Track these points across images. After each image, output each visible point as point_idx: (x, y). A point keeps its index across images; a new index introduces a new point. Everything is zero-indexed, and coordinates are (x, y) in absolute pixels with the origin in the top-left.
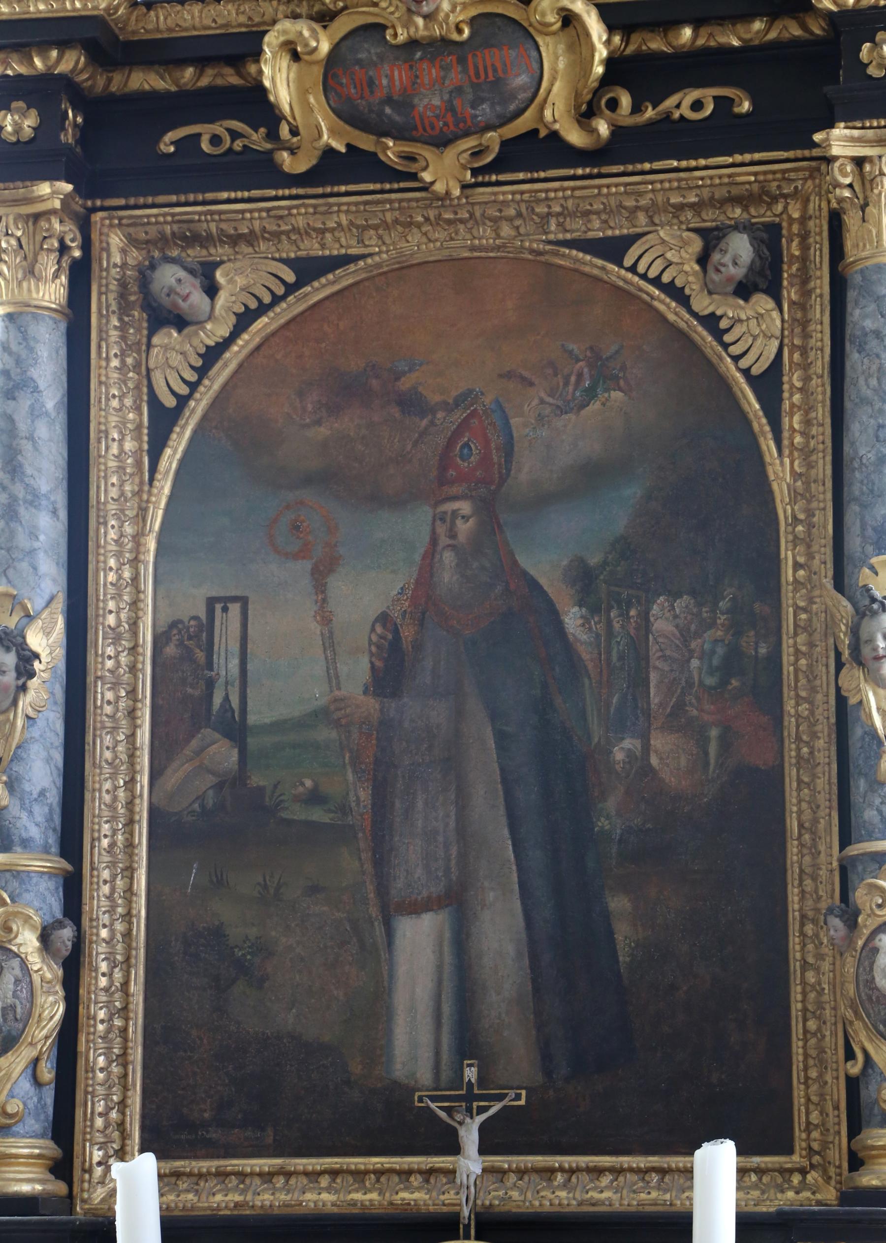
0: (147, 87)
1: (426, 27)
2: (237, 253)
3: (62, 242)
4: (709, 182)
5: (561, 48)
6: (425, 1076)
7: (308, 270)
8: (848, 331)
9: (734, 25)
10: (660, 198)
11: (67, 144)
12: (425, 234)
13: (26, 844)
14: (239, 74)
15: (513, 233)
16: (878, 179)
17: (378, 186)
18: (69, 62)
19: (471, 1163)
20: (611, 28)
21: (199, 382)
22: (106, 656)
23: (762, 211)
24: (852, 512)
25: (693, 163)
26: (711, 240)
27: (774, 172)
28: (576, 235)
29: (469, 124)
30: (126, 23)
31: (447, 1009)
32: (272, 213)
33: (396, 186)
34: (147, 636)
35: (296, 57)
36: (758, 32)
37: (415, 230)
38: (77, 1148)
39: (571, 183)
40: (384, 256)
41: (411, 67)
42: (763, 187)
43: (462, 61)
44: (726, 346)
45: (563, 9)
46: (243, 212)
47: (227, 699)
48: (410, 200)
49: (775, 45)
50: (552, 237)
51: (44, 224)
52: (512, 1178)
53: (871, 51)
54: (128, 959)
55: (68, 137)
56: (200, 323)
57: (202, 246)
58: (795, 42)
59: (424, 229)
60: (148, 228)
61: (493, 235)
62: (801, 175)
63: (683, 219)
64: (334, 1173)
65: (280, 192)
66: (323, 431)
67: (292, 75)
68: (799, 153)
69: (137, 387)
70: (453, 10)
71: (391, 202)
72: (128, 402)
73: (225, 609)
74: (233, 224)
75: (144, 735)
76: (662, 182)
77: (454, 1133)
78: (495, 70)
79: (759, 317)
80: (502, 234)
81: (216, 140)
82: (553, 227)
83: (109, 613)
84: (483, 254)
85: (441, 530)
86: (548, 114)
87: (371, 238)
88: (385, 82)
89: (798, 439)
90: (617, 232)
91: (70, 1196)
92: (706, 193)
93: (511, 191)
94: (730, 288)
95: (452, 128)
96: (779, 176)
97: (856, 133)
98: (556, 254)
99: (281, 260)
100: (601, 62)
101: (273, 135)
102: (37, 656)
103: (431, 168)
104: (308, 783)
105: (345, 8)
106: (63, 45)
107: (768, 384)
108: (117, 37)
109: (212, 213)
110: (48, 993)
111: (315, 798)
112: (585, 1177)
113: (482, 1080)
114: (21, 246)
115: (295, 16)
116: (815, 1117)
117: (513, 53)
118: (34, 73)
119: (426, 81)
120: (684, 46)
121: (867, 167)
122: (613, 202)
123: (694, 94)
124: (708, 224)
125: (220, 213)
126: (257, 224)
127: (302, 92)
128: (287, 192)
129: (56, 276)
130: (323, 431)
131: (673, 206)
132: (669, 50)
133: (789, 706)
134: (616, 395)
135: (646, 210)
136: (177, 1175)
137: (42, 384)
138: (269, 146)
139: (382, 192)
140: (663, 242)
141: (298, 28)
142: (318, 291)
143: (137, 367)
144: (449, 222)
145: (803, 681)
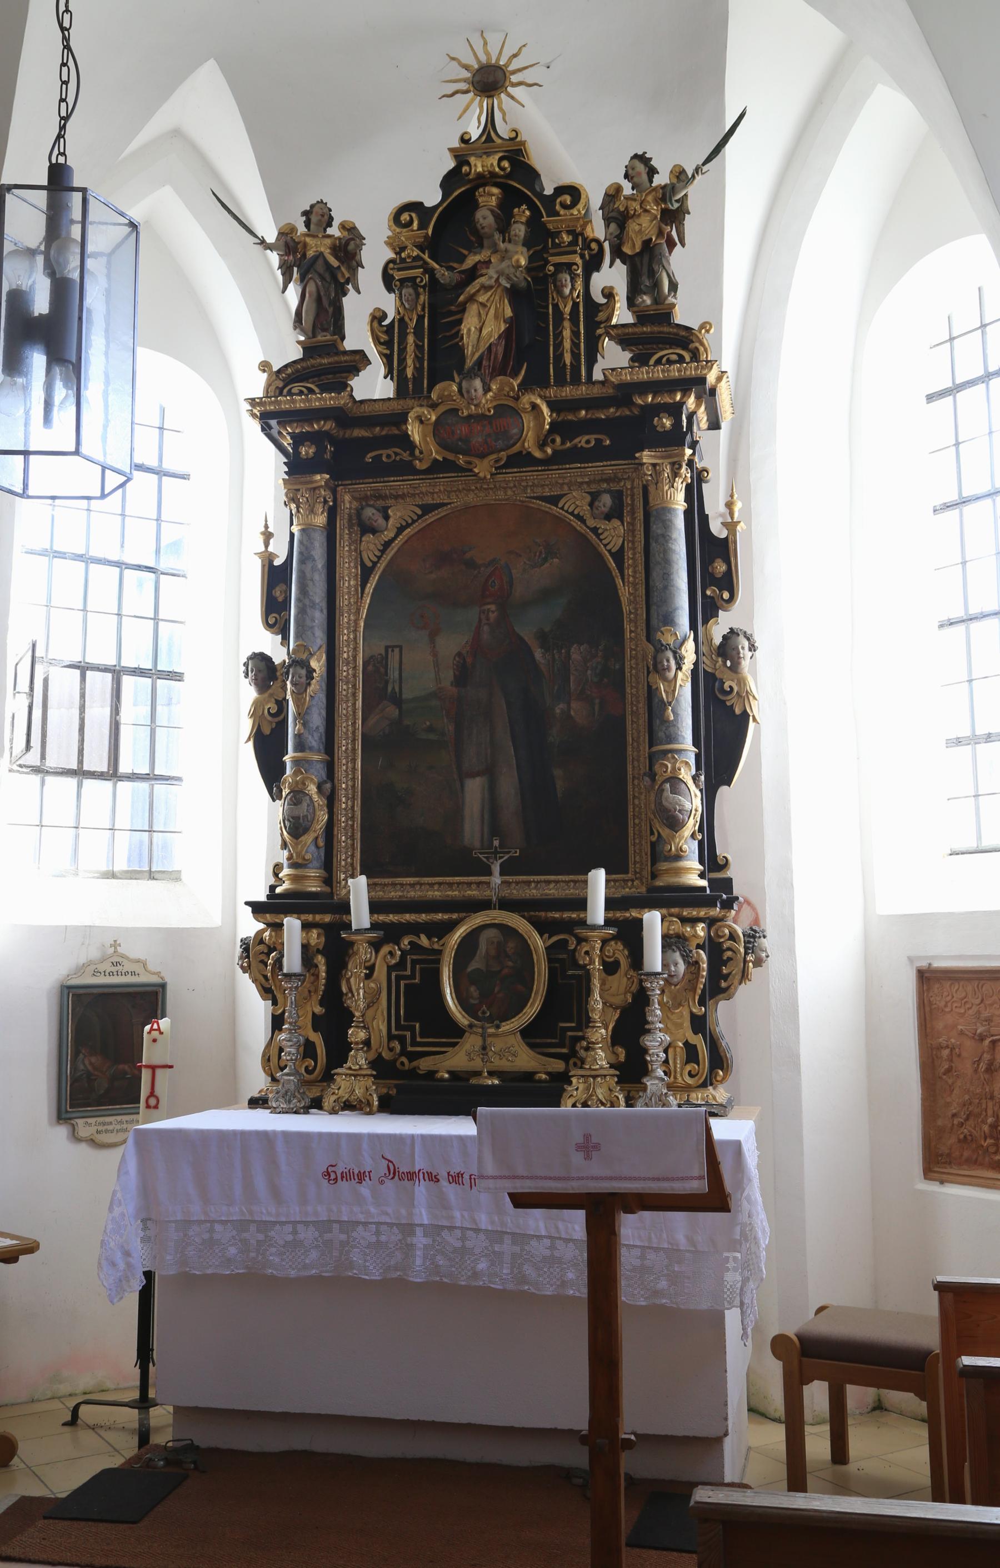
3: (325, 499)
5: (531, 418)
6: (477, 844)
7: (427, 509)
8: (651, 534)
13: (311, 749)
14: (399, 430)
18: (328, 426)
19: (496, 879)
20: (552, 410)
21: (381, 556)
22: (343, 671)
24: (654, 608)
26: (595, 496)
31: (486, 817)
35: (421, 422)
38: (334, 874)
44: (601, 540)
47: (393, 688)
51: (317, 492)
52: (514, 885)
54: (354, 796)
56: (382, 532)
58: (627, 416)
64: (440, 884)
66: (433, 576)
69: (356, 558)
72: (352, 565)
73: (393, 651)
75: (359, 703)
77: (490, 867)
79: (615, 528)
81: (388, 456)
83: (345, 653)
85: (483, 617)
86: (526, 445)
87: (453, 495)
89: (631, 579)
91: (332, 893)
92: (592, 477)
93: (511, 476)
94: (603, 516)
101: (412, 454)
102: (315, 671)
104: (428, 723)
106: (326, 419)
107: (619, 556)
110: (321, 810)
111: (431, 729)
112: (544, 884)
113: (501, 846)
115: (421, 406)
116: (638, 859)
123: (586, 437)
127: (424, 436)
129: (322, 513)
130: (433, 576)
133: (628, 690)
134: (556, 560)
135: (567, 484)
136: (375, 884)
137: (316, 558)
142: (431, 518)
143: (356, 550)
144: (485, 489)
145: (633, 679)
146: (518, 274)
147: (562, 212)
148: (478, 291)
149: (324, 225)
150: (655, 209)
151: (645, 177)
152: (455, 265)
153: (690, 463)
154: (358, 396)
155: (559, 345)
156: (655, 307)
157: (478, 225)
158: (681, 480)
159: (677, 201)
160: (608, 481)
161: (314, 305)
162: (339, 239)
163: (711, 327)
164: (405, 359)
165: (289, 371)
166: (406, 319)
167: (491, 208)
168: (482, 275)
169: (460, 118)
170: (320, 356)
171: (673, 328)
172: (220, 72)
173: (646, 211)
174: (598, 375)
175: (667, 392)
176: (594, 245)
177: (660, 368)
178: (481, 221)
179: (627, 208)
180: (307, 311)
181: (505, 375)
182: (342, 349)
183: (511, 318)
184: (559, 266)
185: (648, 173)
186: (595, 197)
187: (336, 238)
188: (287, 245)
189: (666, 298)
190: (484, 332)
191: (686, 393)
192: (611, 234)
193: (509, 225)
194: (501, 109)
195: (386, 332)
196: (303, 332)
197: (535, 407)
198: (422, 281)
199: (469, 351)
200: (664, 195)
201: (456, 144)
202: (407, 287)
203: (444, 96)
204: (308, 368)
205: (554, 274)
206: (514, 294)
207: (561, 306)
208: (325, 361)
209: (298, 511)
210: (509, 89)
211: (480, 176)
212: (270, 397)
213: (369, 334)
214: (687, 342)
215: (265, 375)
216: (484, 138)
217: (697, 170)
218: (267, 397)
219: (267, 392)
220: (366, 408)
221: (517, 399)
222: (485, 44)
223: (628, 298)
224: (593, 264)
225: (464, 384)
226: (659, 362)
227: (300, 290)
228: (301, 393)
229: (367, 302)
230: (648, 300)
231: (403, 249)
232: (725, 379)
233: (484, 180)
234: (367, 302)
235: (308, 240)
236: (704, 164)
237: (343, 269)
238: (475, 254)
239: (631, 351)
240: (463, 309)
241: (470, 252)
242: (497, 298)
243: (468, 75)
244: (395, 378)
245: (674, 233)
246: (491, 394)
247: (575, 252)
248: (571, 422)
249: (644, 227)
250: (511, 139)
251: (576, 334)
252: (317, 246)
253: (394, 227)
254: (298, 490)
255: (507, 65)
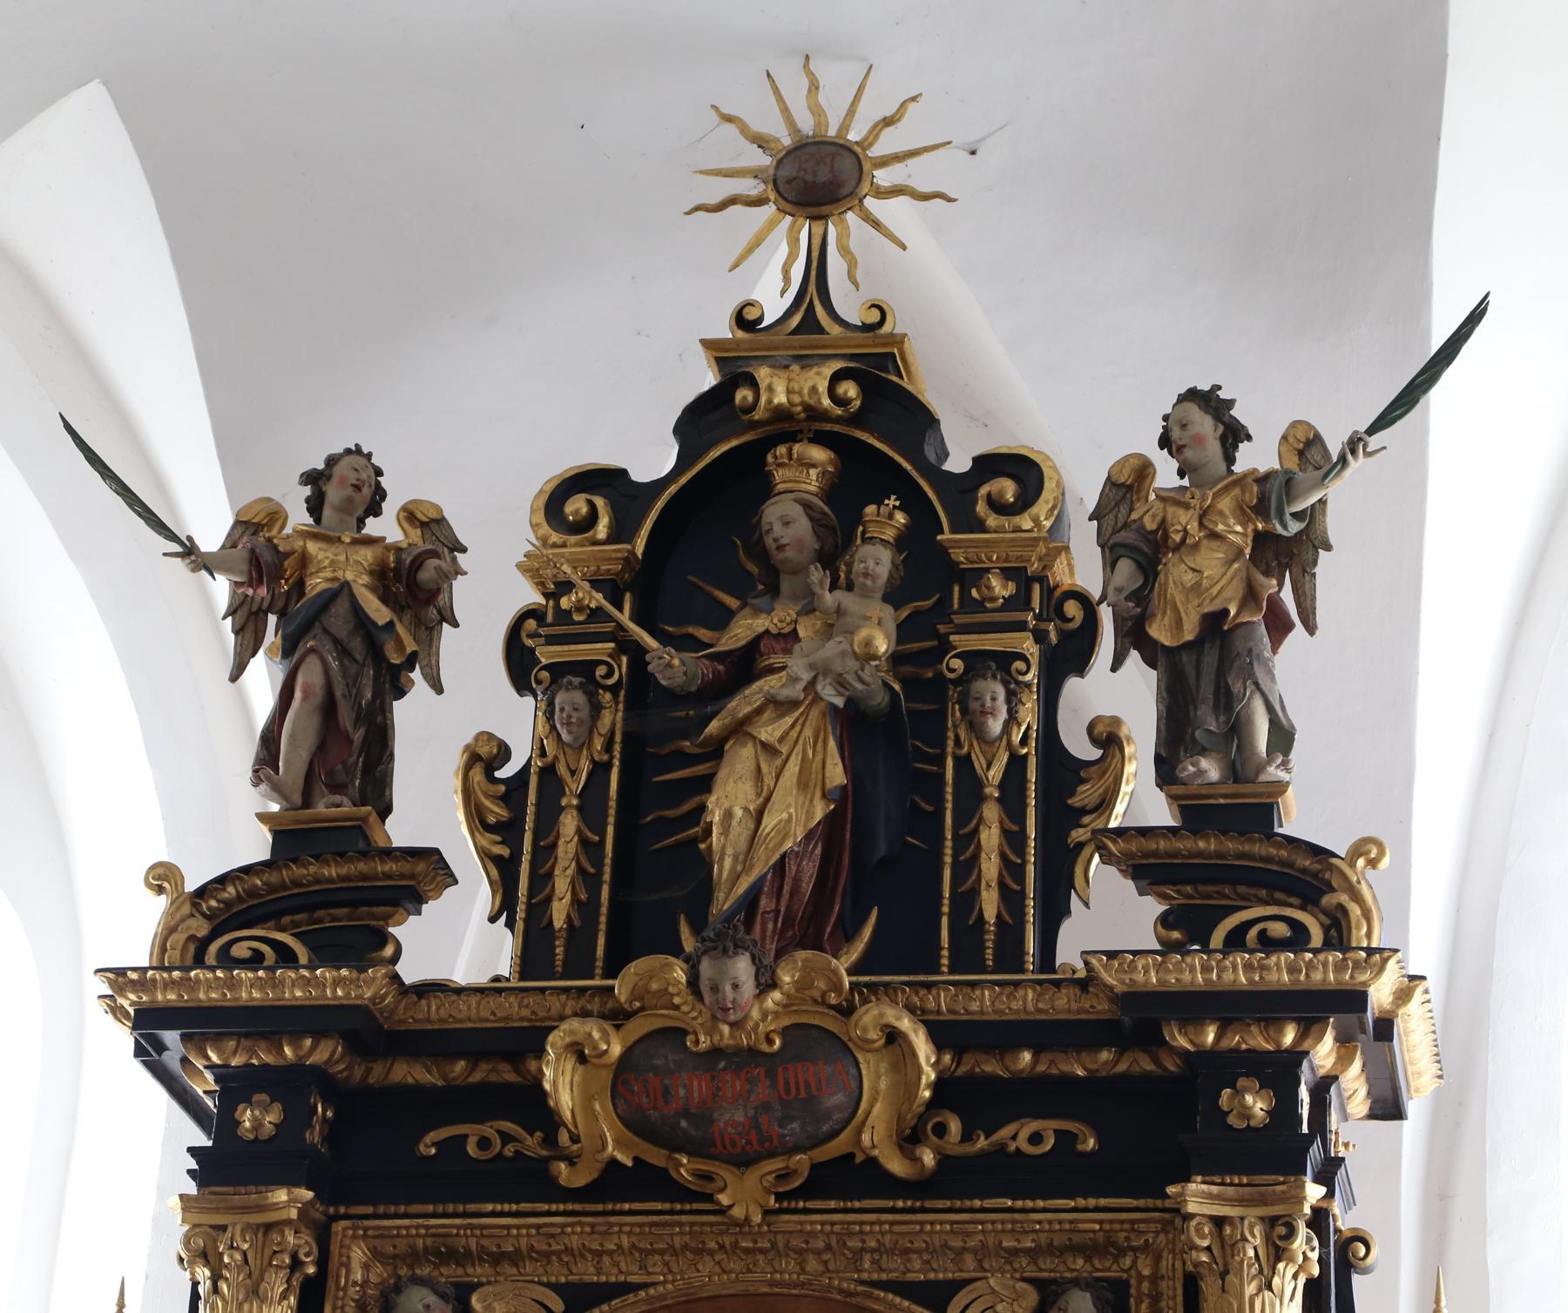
0: (410, 1080)
1: (732, 1035)
2: (498, 1274)
4: (1047, 1227)
5: (883, 1067)
9: (1078, 1053)
10: (991, 1240)
11: (312, 1144)
12: (719, 1263)
14: (516, 1070)
15: (821, 1268)
16: (1240, 1245)
17: (667, 1206)
18: (323, 1053)
20: (939, 1044)
23: (1108, 1264)
25: (1030, 1204)
27: (1122, 1222)
28: (893, 1275)
29: (776, 1143)
30: (393, 1012)
32: (543, 1230)
33: (688, 1207)
35: (582, 1059)
36: (1106, 1063)
37: (707, 1258)
39: (890, 1217)
40: (670, 1286)
41: (713, 1078)
42: (1108, 1238)
43: (771, 1074)
45: (887, 1026)
46: (508, 1227)
48: (703, 1224)
49: (1125, 1077)
50: (865, 1276)
51: (276, 1237)
53: (1231, 1098)
55: (314, 1136)
57: (458, 1264)
58: (1146, 1077)
59: (717, 1258)
60: (397, 1241)
61: (797, 1269)
62: (1152, 1227)
63: (1017, 1266)
65: (554, 1207)
67: (576, 1078)
68: (1150, 1202)
70: (764, 1019)
71: (681, 1224)
74: (496, 1241)
76: (993, 1222)
78: (808, 1085)
80: (808, 1269)
81: (484, 1143)
82: (867, 1265)
84: (785, 1291)
86: (866, 1138)
88: (682, 1092)
90: (941, 1276)
93: (821, 1220)
95: (756, 1146)
96: (1127, 1226)
97: (1215, 1189)
98: (870, 1296)
99: (548, 1285)
100: (928, 1086)
101: (550, 1141)
103: (728, 1191)
105: (642, 1009)
106: (319, 1035)
108: (381, 1026)
109: (472, 1227)
114: (246, 1261)
115: (584, 1014)
117: (829, 1069)
118: (281, 1062)
119: (729, 1094)
120: (1022, 1071)
121: (1228, 1230)
122: (936, 1240)
123: (1033, 1126)
124: (1046, 1275)
125: (482, 1227)
126: (524, 1242)
127: (586, 1098)
128: (561, 1207)
129: (284, 1296)
131: (1006, 1250)
132: (1006, 1075)
135: (974, 1251)
138: (544, 1153)
139: (671, 1212)
140: (994, 1291)
141: (587, 1029)
144: (747, 1251)
146: (867, 675)
147: (992, 521)
148: (759, 711)
149: (360, 512)
150: (1238, 532)
151: (1214, 448)
152: (703, 634)
153: (1319, 1220)
154: (410, 972)
155: (967, 866)
156: (1231, 788)
157: (769, 541)
158: (1291, 1270)
159: (1297, 516)
160: (1089, 1250)
161: (313, 724)
162: (398, 550)
163: (1382, 853)
164: (550, 875)
165: (231, 891)
166: (562, 769)
167: (803, 489)
168: (772, 670)
169: (735, 266)
170: (317, 857)
171: (1279, 846)
172: (116, 115)
173: (1214, 535)
174: (1070, 948)
175: (1258, 1020)
176: (1072, 609)
177: (1240, 958)
178: (778, 529)
179: (1163, 524)
180: (292, 736)
181: (818, 947)
182: (382, 844)
183: (844, 788)
184: (976, 660)
185: (1223, 439)
186: (1080, 480)
187: (388, 548)
188: (254, 560)
189: (1261, 768)
190: (769, 822)
191: (1310, 1027)
192: (1119, 590)
193: (848, 541)
194: (844, 251)
195: (504, 799)
196: (278, 790)
197: (893, 1037)
198: (610, 674)
199: (724, 868)
200: (1263, 499)
201: (723, 330)
202: (570, 687)
203: (698, 208)
204: (284, 887)
205: (964, 680)
206: (856, 725)
207: (979, 762)
208: (331, 871)
209: (215, 1290)
210: (870, 203)
211: (781, 415)
212: (169, 969)
213: (458, 799)
214: (1313, 884)
215: (162, 902)
216: (796, 320)
217: (1354, 444)
218: (161, 968)
219: (163, 949)
220: (434, 1011)
221: (846, 1011)
222: (814, 87)
223: (1159, 760)
224: (1070, 655)
225: (706, 968)
226: (1235, 940)
227: (280, 677)
228: (256, 960)
229: (460, 712)
230: (1211, 769)
231: (566, 586)
232: (1418, 996)
233: (789, 426)
234: (460, 712)
235: (312, 547)
236: (1372, 430)
237: (400, 629)
238: (757, 611)
239: (1163, 897)
240: (716, 752)
241: (744, 605)
242: (808, 733)
243: (764, 160)
244: (520, 925)
245: (1287, 595)
246: (776, 995)
247: (1021, 626)
248: (992, 1080)
249: (1206, 577)
250: (867, 328)
251: (1014, 839)
252: (337, 567)
253: (545, 529)
254: (223, 1228)
255: (865, 144)
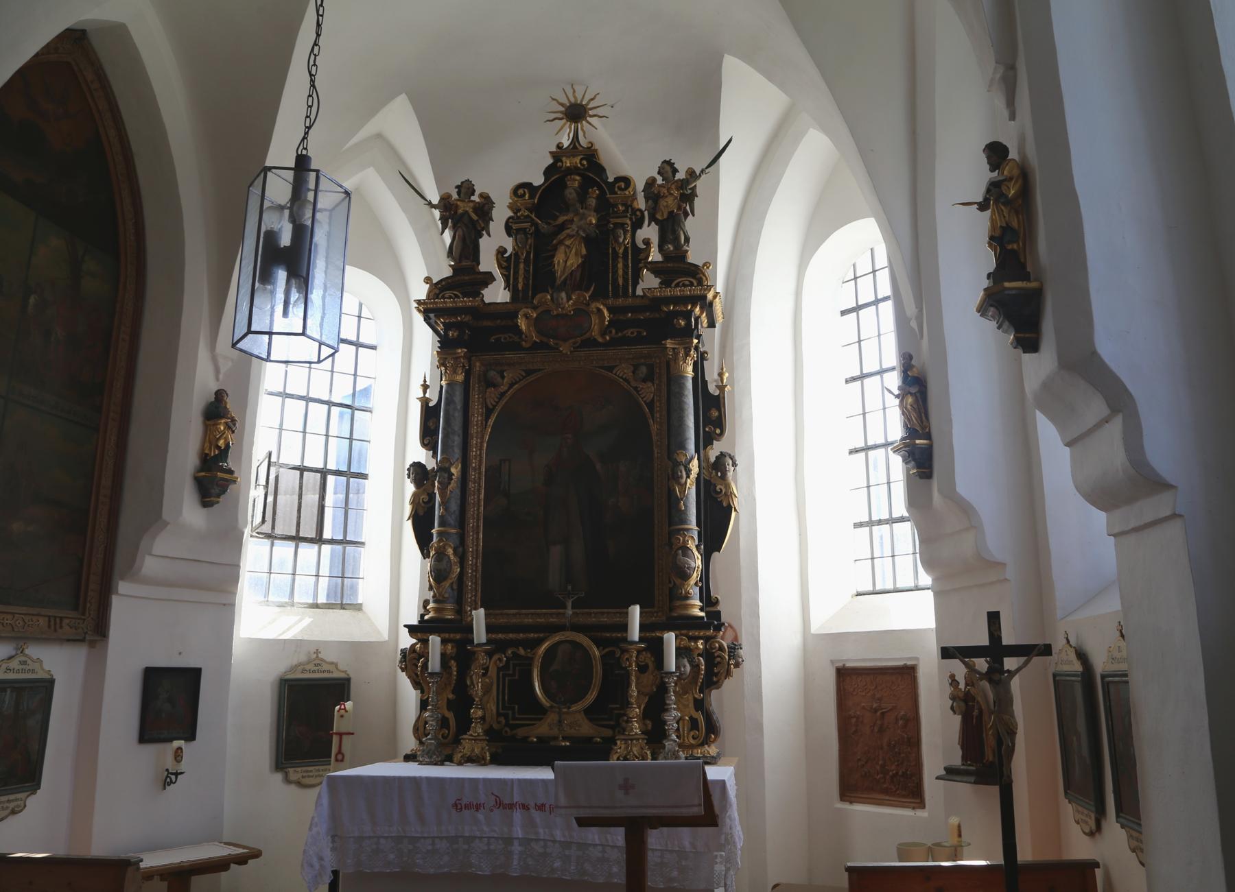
18: (467, 318)
19: (570, 612)
34: (483, 469)
55: (466, 337)
75: (482, 496)
107: (651, 405)
127: (528, 326)
